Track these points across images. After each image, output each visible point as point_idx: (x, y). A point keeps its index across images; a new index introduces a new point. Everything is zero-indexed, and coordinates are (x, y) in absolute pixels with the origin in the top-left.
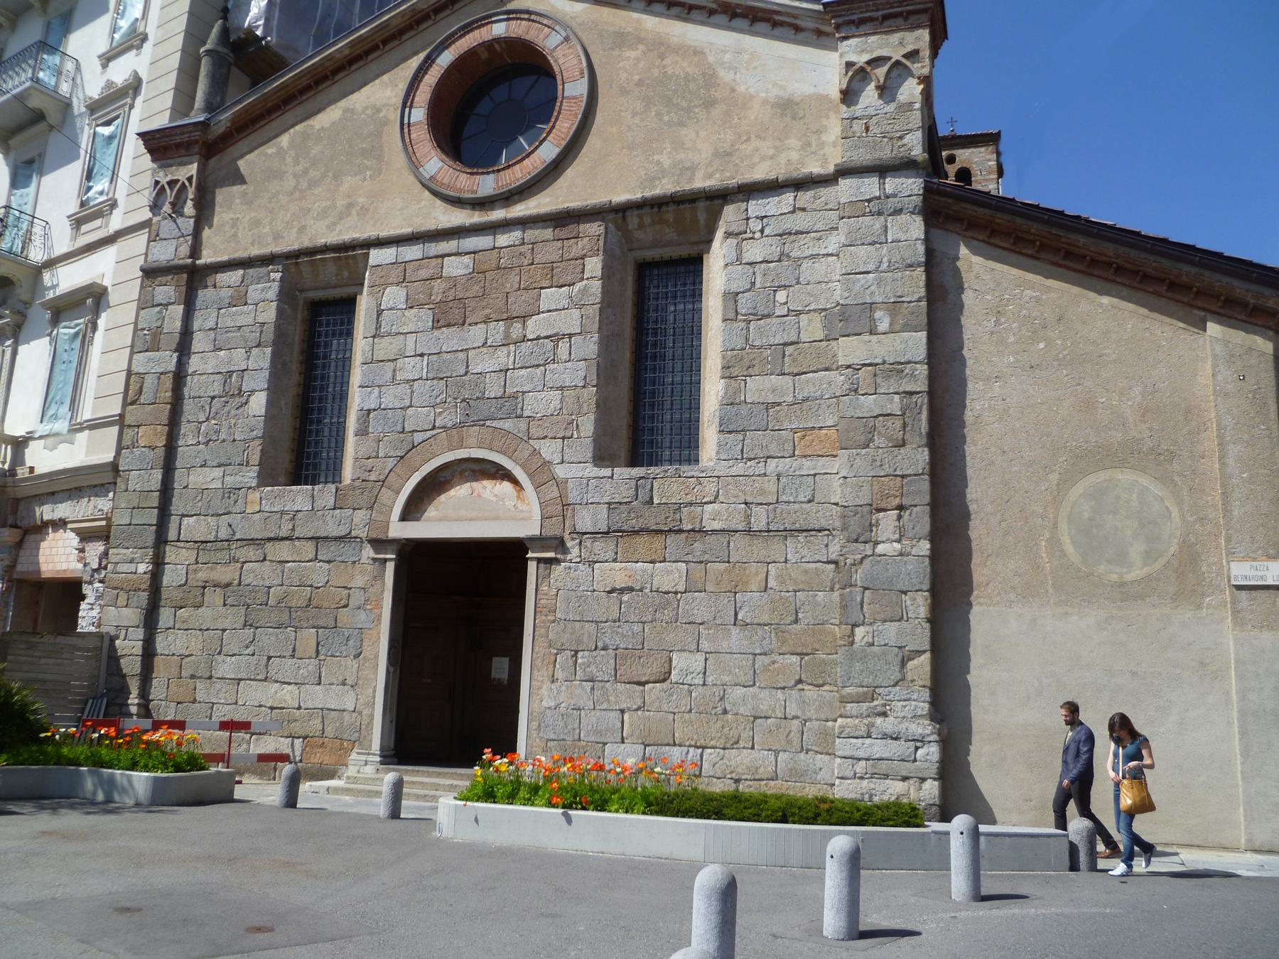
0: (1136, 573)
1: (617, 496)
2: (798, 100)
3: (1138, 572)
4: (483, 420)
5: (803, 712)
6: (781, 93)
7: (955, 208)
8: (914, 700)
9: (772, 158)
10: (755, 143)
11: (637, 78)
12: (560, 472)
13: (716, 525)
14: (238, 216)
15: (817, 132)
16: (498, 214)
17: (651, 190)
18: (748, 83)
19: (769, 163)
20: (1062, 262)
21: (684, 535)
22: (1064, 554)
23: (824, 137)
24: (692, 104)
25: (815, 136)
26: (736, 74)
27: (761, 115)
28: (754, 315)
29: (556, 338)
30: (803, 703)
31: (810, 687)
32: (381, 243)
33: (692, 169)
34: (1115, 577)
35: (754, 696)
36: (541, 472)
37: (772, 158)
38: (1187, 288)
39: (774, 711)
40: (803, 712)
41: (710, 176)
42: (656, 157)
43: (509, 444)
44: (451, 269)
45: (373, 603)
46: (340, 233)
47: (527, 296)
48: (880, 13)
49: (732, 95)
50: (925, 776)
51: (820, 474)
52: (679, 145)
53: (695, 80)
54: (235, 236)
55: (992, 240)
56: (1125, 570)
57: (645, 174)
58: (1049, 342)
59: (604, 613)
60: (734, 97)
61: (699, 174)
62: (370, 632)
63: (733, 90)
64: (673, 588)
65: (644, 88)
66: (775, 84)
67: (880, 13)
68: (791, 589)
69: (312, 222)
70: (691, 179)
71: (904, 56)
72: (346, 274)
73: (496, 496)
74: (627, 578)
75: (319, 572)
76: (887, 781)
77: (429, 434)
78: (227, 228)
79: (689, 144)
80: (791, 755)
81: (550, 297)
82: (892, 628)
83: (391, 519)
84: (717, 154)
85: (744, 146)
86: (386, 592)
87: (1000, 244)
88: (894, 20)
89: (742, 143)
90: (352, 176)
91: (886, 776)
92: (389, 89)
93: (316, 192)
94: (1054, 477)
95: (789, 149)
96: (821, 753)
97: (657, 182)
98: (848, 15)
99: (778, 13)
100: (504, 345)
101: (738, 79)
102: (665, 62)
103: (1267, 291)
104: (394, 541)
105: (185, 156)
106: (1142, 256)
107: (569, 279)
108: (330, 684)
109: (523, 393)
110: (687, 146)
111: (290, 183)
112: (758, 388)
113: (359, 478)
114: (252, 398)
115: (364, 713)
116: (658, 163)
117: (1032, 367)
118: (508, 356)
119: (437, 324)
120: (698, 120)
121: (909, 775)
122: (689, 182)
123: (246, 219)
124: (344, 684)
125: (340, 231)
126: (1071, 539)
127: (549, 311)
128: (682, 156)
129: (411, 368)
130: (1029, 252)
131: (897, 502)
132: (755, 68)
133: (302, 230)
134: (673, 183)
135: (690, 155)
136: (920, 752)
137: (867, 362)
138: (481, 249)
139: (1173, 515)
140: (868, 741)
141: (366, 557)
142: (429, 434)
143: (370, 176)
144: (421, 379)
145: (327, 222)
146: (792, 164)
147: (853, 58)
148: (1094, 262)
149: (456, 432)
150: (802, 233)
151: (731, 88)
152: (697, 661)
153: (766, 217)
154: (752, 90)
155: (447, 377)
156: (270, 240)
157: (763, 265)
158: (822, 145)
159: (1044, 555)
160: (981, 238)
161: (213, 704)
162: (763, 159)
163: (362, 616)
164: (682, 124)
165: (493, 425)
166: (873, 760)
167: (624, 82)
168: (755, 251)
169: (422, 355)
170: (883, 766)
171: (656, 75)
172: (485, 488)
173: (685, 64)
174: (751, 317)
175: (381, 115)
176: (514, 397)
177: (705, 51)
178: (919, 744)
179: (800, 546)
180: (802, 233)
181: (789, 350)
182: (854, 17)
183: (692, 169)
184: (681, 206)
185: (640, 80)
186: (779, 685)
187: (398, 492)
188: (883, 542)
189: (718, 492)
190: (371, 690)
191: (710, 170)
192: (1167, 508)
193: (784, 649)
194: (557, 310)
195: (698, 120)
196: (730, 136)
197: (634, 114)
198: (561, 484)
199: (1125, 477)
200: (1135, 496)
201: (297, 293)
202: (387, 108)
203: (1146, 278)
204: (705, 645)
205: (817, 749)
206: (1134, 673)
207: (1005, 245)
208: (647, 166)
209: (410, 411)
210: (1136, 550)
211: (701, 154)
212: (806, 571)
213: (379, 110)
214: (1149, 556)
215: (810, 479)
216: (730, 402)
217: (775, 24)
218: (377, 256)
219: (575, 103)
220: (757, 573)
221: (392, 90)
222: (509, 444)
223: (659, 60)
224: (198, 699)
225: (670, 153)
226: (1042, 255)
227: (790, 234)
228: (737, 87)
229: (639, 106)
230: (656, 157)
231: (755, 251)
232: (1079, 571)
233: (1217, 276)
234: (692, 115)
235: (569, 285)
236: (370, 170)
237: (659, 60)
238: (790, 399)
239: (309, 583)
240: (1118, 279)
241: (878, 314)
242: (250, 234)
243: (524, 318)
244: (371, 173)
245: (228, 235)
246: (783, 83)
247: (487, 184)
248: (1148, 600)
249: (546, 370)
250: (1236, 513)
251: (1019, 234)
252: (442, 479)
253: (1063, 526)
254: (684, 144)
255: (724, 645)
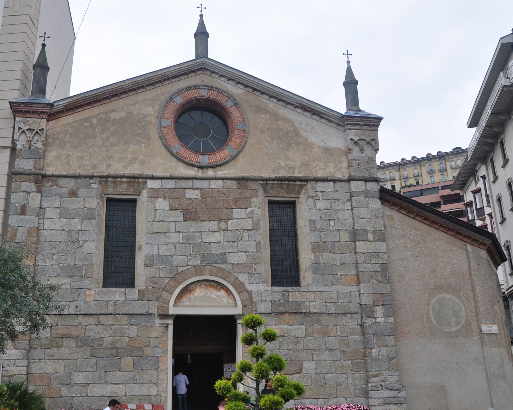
0: (454, 329)
1: (274, 298)
2: (331, 148)
3: (454, 328)
4: (212, 263)
5: (354, 382)
6: (324, 144)
7: (389, 198)
8: (394, 375)
9: (324, 169)
10: (317, 162)
11: (267, 127)
12: (249, 287)
13: (315, 311)
14: (69, 153)
15: (339, 162)
16: (210, 173)
17: (277, 174)
18: (313, 138)
19: (323, 171)
20: (423, 221)
21: (303, 314)
22: (432, 322)
23: (342, 165)
24: (291, 142)
25: (339, 164)
26: (307, 133)
27: (318, 152)
28: (323, 229)
29: (242, 231)
30: (354, 379)
31: (356, 372)
32: (153, 178)
33: (293, 168)
34: (448, 330)
35: (336, 377)
36: (240, 287)
37: (324, 169)
38: (461, 234)
39: (343, 382)
40: (354, 382)
41: (301, 173)
42: (278, 161)
43: (225, 275)
44: (188, 195)
45: (163, 344)
46: (131, 170)
47: (227, 211)
48: (362, 123)
49: (306, 142)
50: (402, 403)
51: (352, 292)
52: (287, 158)
53: (291, 133)
54: (68, 163)
55: (399, 211)
56: (450, 328)
57: (274, 167)
58: (421, 248)
59: (272, 346)
60: (307, 143)
61: (296, 171)
62: (163, 358)
63: (306, 140)
64: (300, 335)
65: (270, 132)
66: (322, 141)
67: (362, 123)
68: (345, 335)
69: (114, 163)
70: (293, 172)
71: (370, 140)
72: (132, 190)
73: (218, 296)
74: (281, 332)
75: (133, 331)
76: (390, 406)
77: (185, 268)
78: (63, 158)
79: (291, 158)
80: (351, 399)
81: (237, 213)
82: (384, 349)
83: (170, 306)
84: (302, 164)
85: (312, 163)
86: (169, 339)
87: (403, 212)
88: (366, 126)
89: (312, 162)
90: (134, 145)
91: (389, 404)
92: (151, 108)
93: (115, 149)
94: (426, 295)
95: (330, 167)
96: (362, 397)
97: (280, 172)
98: (351, 121)
99: (323, 114)
100: (218, 231)
101: (308, 136)
102: (278, 123)
103: (485, 239)
104: (171, 316)
105: (37, 118)
106: (449, 223)
107: (245, 206)
108: (142, 383)
109: (229, 253)
110: (290, 159)
111: (99, 142)
112: (325, 258)
113: (150, 286)
114: (85, 244)
115: (162, 396)
116: (279, 164)
117: (416, 257)
118: (220, 236)
119: (185, 219)
120: (294, 149)
121: (397, 403)
122: (292, 174)
123: (75, 155)
124: (150, 383)
125: (130, 169)
126: (434, 317)
127: (237, 219)
128: (289, 162)
129: (175, 238)
130: (412, 216)
131: (381, 303)
132: (314, 133)
133: (109, 166)
134: (286, 173)
135: (292, 163)
136: (400, 394)
137: (367, 251)
138: (203, 188)
139: (463, 310)
140: (382, 391)
141: (157, 323)
142: (185, 268)
143: (144, 146)
144: (179, 243)
145: (123, 164)
146: (331, 173)
147: (353, 137)
148: (433, 222)
149: (198, 270)
150: (337, 200)
151: (306, 139)
152: (313, 365)
153: (323, 192)
154: (314, 141)
155: (192, 243)
156: (90, 168)
157: (324, 211)
158: (342, 167)
159: (426, 322)
160: (396, 209)
161: (73, 397)
162: (321, 169)
163: (158, 350)
164: (287, 150)
165: (216, 266)
166: (384, 398)
167: (262, 127)
168: (320, 205)
169: (179, 232)
170: (388, 400)
171: (275, 127)
172: (212, 293)
173: (287, 126)
174: (321, 230)
175: (147, 119)
176: (225, 254)
177: (294, 122)
178: (399, 391)
179: (347, 319)
180: (337, 200)
181: (336, 244)
182: (353, 123)
183: (293, 168)
184: (283, 182)
185: (268, 128)
186: (345, 372)
187: (172, 294)
188: (378, 318)
189: (315, 297)
190: (165, 385)
191: (300, 170)
192: (461, 307)
193: (345, 359)
194: (241, 219)
195: (294, 149)
196: (307, 158)
197: (267, 142)
198: (250, 293)
199: (448, 296)
200: (451, 303)
201: (104, 195)
202: (150, 116)
203: (449, 229)
204: (315, 358)
205: (360, 396)
206: (457, 363)
207: (404, 213)
208: (275, 164)
209: (175, 257)
210: (453, 321)
211: (296, 163)
212: (350, 329)
213: (146, 117)
214: (458, 323)
215: (349, 294)
216: (316, 262)
217: (322, 117)
218: (151, 184)
219: (242, 132)
220: (332, 329)
221: (152, 109)
222: (225, 275)
223: (276, 122)
224: (63, 395)
225: (283, 160)
226: (416, 218)
227: (333, 199)
228: (308, 139)
229: (269, 139)
230: (278, 161)
231: (320, 205)
232: (437, 328)
233: (471, 232)
234: (291, 146)
235: (245, 209)
236: (144, 143)
237: (276, 122)
238: (339, 263)
239: (127, 335)
240: (440, 229)
241: (369, 234)
242: (77, 163)
243: (227, 220)
244: (145, 145)
245: (64, 162)
246: (325, 141)
247: (205, 160)
248: (458, 338)
249: (238, 244)
250: (481, 309)
251: (410, 210)
252: (191, 288)
253: (431, 313)
254: (289, 158)
255: (322, 358)
